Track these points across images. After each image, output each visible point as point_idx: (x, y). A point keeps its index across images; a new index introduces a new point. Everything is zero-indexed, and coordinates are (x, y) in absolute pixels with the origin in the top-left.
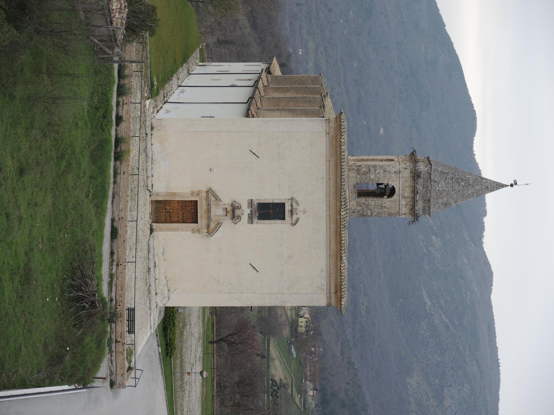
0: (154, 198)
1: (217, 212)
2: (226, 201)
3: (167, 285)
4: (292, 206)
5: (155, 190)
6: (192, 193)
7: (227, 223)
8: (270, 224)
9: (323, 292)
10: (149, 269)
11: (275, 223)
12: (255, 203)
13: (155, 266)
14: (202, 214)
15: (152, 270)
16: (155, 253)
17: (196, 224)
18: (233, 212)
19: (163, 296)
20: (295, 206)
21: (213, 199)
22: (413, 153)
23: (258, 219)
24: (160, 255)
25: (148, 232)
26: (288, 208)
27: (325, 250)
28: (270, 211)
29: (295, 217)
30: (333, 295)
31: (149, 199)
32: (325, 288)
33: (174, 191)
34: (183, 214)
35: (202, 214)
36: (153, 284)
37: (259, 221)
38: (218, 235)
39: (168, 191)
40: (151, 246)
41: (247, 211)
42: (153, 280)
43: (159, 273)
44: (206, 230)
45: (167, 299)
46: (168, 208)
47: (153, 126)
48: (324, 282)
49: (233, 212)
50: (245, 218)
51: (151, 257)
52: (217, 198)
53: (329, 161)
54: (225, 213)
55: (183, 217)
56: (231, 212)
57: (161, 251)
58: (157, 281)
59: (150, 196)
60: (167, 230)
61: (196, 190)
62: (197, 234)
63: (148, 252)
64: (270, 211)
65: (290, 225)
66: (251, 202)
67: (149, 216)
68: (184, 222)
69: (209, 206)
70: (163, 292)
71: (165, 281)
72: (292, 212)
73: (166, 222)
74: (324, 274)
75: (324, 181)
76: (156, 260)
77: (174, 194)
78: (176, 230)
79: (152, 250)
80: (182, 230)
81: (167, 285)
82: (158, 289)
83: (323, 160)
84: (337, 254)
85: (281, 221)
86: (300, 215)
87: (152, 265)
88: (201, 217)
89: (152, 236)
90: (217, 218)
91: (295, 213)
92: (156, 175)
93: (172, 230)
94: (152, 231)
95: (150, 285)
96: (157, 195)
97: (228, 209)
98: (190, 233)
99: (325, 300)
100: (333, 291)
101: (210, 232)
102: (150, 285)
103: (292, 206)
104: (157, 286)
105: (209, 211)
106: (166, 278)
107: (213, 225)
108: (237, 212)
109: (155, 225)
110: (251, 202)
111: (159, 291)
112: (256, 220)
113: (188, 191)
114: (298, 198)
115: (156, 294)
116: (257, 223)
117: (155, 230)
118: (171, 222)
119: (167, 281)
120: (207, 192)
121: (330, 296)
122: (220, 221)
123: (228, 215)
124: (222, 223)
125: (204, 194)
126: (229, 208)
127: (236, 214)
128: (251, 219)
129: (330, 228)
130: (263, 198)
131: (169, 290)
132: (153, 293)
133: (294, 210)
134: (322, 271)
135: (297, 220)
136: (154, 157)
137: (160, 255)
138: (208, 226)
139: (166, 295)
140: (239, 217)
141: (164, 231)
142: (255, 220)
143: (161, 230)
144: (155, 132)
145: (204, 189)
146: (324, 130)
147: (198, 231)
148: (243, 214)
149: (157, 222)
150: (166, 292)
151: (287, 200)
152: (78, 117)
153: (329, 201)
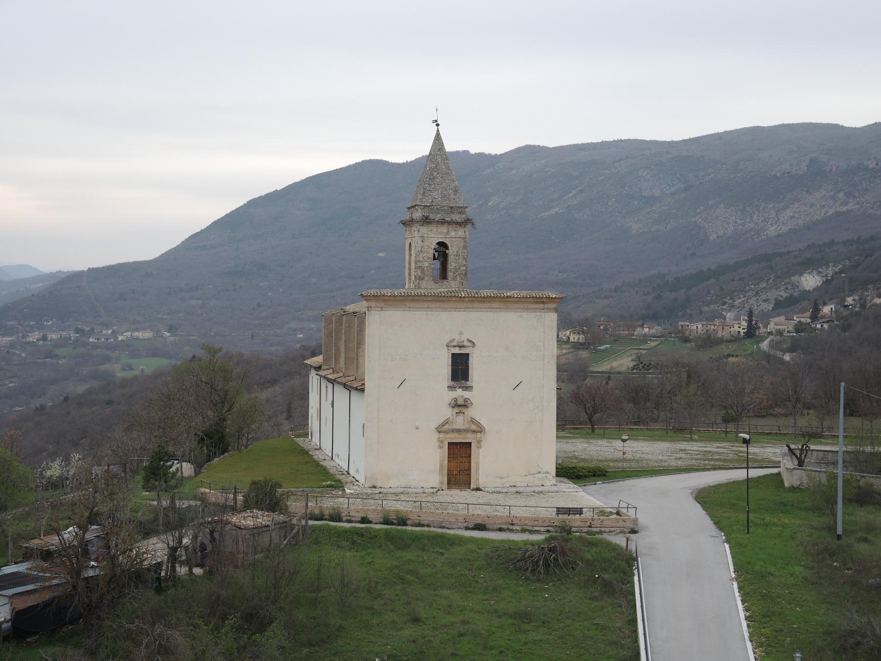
0: (445, 486)
1: (460, 422)
2: (449, 413)
4: (455, 346)
5: (436, 485)
6: (441, 447)
7: (471, 412)
12: (451, 383)
15: (518, 489)
18: (461, 406)
20: (455, 343)
21: (447, 426)
26: (457, 351)
28: (460, 368)
31: (446, 491)
36: (533, 489)
38: (483, 422)
41: (459, 392)
44: (479, 434)
46: (455, 472)
48: (533, 315)
49: (461, 406)
50: (466, 394)
51: (505, 490)
52: (446, 422)
57: (499, 480)
60: (477, 473)
61: (437, 444)
64: (460, 368)
66: (451, 388)
68: (470, 456)
69: (453, 431)
73: (469, 474)
74: (525, 314)
77: (441, 466)
78: (477, 464)
80: (478, 458)
86: (464, 338)
87: (513, 490)
92: (422, 484)
93: (478, 469)
94: (478, 489)
96: (442, 483)
100: (541, 306)
101: (480, 430)
103: (455, 346)
105: (459, 431)
107: (474, 427)
108: (460, 402)
109: (472, 486)
110: (451, 388)
111: (540, 483)
113: (438, 451)
114: (447, 340)
118: (470, 470)
120: (439, 432)
125: (442, 435)
128: (468, 388)
132: (541, 489)
134: (521, 316)
138: (474, 432)
140: (466, 400)
143: (478, 479)
144: (378, 485)
145: (437, 435)
147: (479, 442)
149: (470, 484)
150: (540, 476)
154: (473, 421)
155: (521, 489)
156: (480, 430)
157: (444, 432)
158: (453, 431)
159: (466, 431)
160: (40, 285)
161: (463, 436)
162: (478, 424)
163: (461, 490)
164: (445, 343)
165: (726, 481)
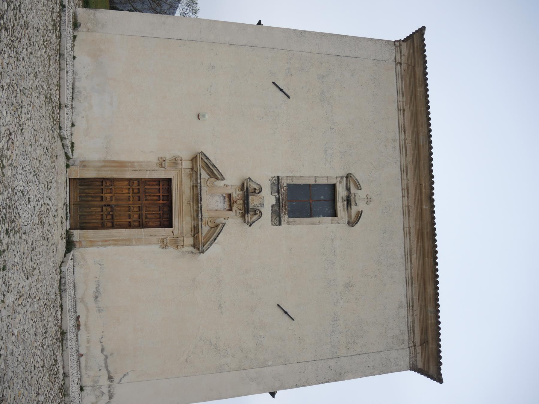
0: (77, 173)
1: (213, 202)
2: (232, 181)
3: (106, 367)
4: (348, 189)
5: (78, 155)
6: (161, 164)
7: (233, 223)
8: (313, 224)
9: (402, 346)
10: (63, 333)
11: (320, 223)
12: (284, 183)
13: (78, 327)
14: (181, 206)
15: (70, 335)
16: (78, 296)
17: (170, 229)
18: (244, 203)
19: (98, 393)
20: (353, 190)
21: (204, 175)
22: (107, 148)
23: (289, 217)
24: (90, 301)
25: (62, 244)
26: (341, 193)
27: (403, 268)
28: (307, 201)
29: (354, 210)
30: (419, 349)
31: (62, 178)
32: (406, 338)
33: (123, 158)
34: (140, 209)
35: (181, 206)
36: (73, 371)
37: (291, 220)
38: (215, 250)
39: (109, 158)
40: (69, 277)
41: (268, 199)
42: (71, 361)
43: (88, 342)
44: (191, 241)
45: (106, 398)
46: (107, 196)
47: (79, 21)
48: (404, 327)
49: (244, 203)
50: (267, 212)
51: (68, 304)
52: (214, 173)
53: (404, 110)
54: (227, 206)
55: (140, 216)
56: (241, 202)
57: (92, 289)
58: (83, 359)
59: (67, 166)
60: (105, 243)
61: (168, 156)
62: (171, 250)
63: (61, 291)
64: (307, 201)
65: (346, 226)
66: (277, 182)
67: (62, 213)
68: (142, 226)
69: (197, 187)
70: (96, 382)
71: (101, 358)
72: (348, 200)
73: (103, 226)
74: (404, 312)
75: (397, 144)
76: (81, 311)
77: (122, 165)
78: (127, 242)
79: (69, 286)
80: (139, 242)
81: (106, 367)
82: (85, 378)
83: (394, 107)
84: (424, 275)
85: (329, 219)
86: (361, 206)
87: (69, 324)
88: (181, 212)
89: (70, 255)
90: (213, 214)
91: (353, 203)
92: (81, 124)
93: (116, 243)
94: (70, 245)
95: (65, 375)
96: (84, 165)
97: (234, 196)
98: (156, 248)
99: (408, 360)
100: (418, 341)
101: (200, 240)
102: (65, 375)
103: (348, 189)
104: (83, 371)
105: (197, 199)
106: (102, 350)
107: (205, 230)
108: (253, 201)
109: (77, 234)
110: (277, 182)
111: (87, 382)
112: (286, 216)
113: (153, 159)
114: (359, 175)
115: (82, 389)
116: (288, 223)
117: (77, 245)
118: (113, 226)
119: (106, 357)
120: (194, 160)
121: (415, 350)
122: (218, 221)
123: (235, 207)
124: (224, 224)
125: (187, 165)
126: (237, 195)
127: (251, 207)
128: (277, 219)
129: (410, 228)
130: (297, 175)
131: (110, 378)
132: (74, 388)
133: (352, 197)
134: (400, 307)
135: (359, 215)
136: (77, 84)
137: (90, 301)
138: (196, 231)
139: (105, 390)
140: (257, 212)
141: (97, 246)
142: (285, 218)
143: (92, 243)
144: (81, 34)
145: (185, 155)
146: (393, 58)
147: (175, 242)
148: (262, 205)
149: (82, 228)
150: (104, 381)
151: (339, 179)
152: (6, 55)
153: (407, 180)
154: (217, 228)
155: (71, 342)
156: (199, 245)
157: (193, 170)
158: (197, 187)
159: (197, 214)
160: (415, 256)
161: (187, 209)
162: (212, 237)
163: (68, 207)
164: (352, 171)
165: (316, 219)
